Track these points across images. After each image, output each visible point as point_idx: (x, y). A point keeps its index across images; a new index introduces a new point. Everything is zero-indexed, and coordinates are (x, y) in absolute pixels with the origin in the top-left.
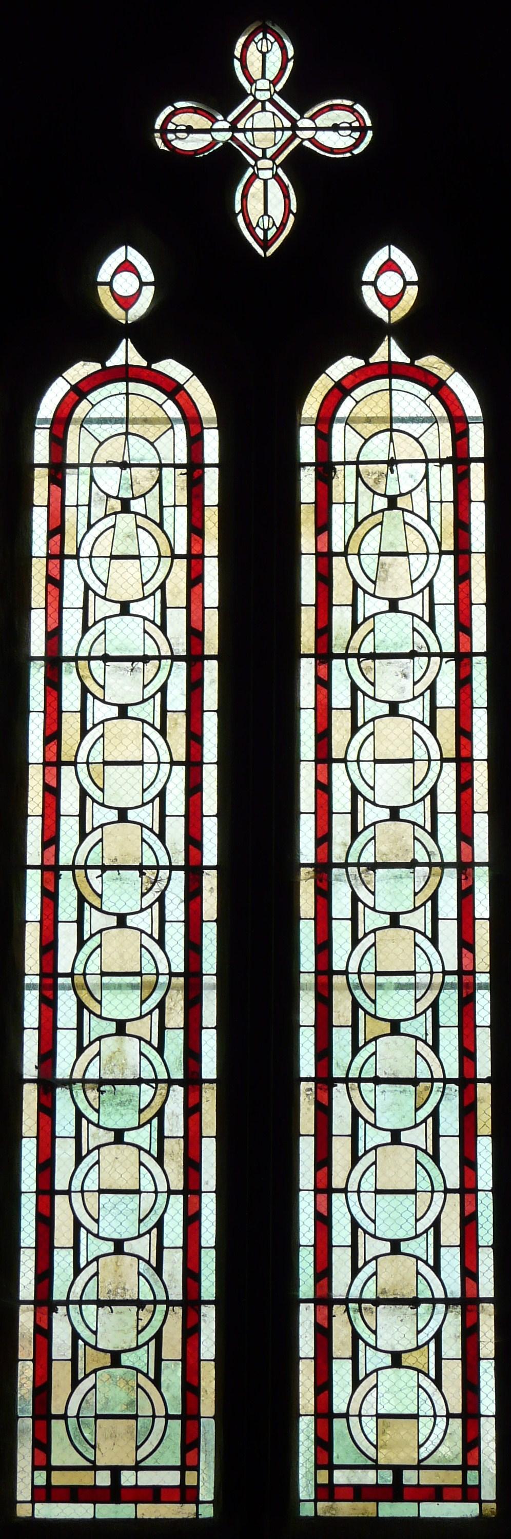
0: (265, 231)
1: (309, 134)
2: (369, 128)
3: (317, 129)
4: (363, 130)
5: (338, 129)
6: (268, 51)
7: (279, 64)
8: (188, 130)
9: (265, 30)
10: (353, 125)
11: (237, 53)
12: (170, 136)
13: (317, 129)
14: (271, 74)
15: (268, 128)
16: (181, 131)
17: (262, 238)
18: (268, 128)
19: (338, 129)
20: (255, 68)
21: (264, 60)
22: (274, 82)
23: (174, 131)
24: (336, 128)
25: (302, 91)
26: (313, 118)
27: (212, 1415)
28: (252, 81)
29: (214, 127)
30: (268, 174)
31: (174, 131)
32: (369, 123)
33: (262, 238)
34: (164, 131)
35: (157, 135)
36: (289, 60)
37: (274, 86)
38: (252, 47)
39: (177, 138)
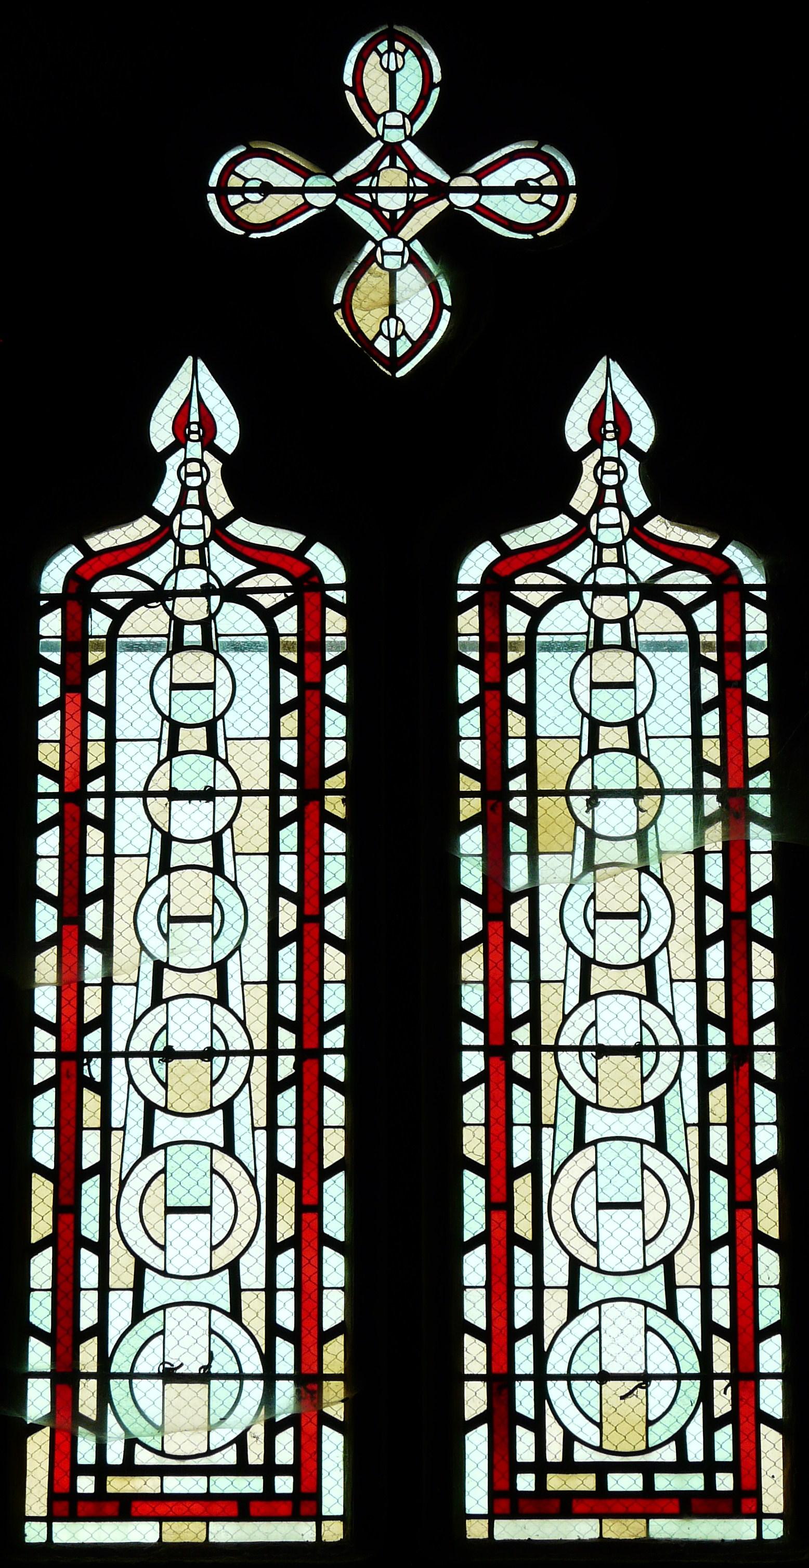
0: (393, 343)
1: (313, 182)
2: (212, 190)
3: (302, 191)
4: (562, 190)
5: (519, 191)
6: (398, 70)
7: (416, 95)
8: (264, 190)
9: (392, 37)
10: (545, 182)
11: (348, 80)
12: (551, 181)
13: (302, 191)
14: (407, 103)
15: (398, 203)
16: (253, 190)
17: (387, 354)
18: (398, 203)
19: (519, 191)
20: (378, 100)
21: (393, 83)
22: (413, 117)
23: (241, 191)
24: (521, 188)
25: (457, 135)
26: (307, 206)
27: (342, 1284)
28: (373, 118)
29: (476, 196)
30: (394, 119)
31: (241, 191)
32: (211, 198)
33: (387, 354)
34: (223, 191)
35: (211, 198)
36: (434, 86)
37: (412, 125)
38: (373, 58)
39: (246, 201)
